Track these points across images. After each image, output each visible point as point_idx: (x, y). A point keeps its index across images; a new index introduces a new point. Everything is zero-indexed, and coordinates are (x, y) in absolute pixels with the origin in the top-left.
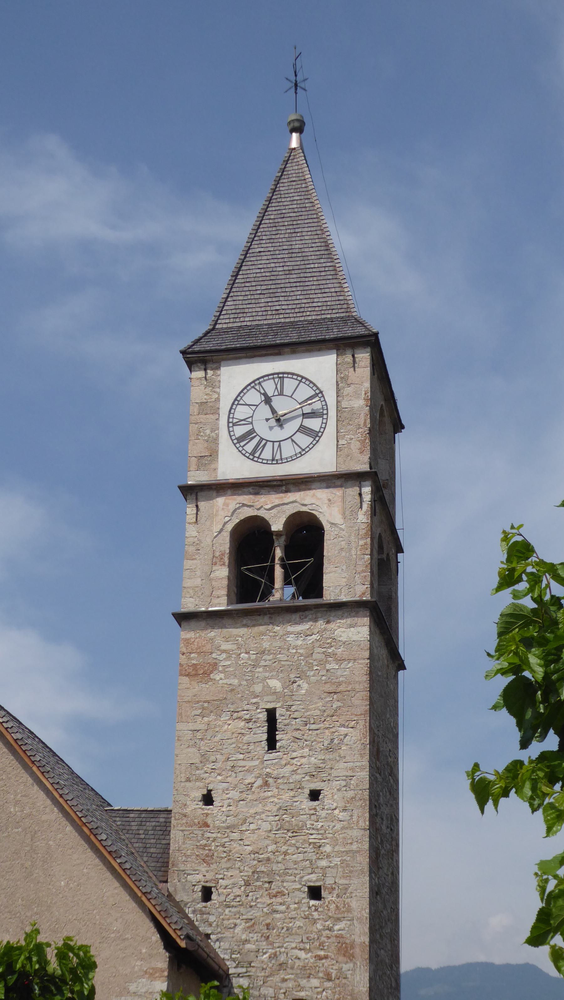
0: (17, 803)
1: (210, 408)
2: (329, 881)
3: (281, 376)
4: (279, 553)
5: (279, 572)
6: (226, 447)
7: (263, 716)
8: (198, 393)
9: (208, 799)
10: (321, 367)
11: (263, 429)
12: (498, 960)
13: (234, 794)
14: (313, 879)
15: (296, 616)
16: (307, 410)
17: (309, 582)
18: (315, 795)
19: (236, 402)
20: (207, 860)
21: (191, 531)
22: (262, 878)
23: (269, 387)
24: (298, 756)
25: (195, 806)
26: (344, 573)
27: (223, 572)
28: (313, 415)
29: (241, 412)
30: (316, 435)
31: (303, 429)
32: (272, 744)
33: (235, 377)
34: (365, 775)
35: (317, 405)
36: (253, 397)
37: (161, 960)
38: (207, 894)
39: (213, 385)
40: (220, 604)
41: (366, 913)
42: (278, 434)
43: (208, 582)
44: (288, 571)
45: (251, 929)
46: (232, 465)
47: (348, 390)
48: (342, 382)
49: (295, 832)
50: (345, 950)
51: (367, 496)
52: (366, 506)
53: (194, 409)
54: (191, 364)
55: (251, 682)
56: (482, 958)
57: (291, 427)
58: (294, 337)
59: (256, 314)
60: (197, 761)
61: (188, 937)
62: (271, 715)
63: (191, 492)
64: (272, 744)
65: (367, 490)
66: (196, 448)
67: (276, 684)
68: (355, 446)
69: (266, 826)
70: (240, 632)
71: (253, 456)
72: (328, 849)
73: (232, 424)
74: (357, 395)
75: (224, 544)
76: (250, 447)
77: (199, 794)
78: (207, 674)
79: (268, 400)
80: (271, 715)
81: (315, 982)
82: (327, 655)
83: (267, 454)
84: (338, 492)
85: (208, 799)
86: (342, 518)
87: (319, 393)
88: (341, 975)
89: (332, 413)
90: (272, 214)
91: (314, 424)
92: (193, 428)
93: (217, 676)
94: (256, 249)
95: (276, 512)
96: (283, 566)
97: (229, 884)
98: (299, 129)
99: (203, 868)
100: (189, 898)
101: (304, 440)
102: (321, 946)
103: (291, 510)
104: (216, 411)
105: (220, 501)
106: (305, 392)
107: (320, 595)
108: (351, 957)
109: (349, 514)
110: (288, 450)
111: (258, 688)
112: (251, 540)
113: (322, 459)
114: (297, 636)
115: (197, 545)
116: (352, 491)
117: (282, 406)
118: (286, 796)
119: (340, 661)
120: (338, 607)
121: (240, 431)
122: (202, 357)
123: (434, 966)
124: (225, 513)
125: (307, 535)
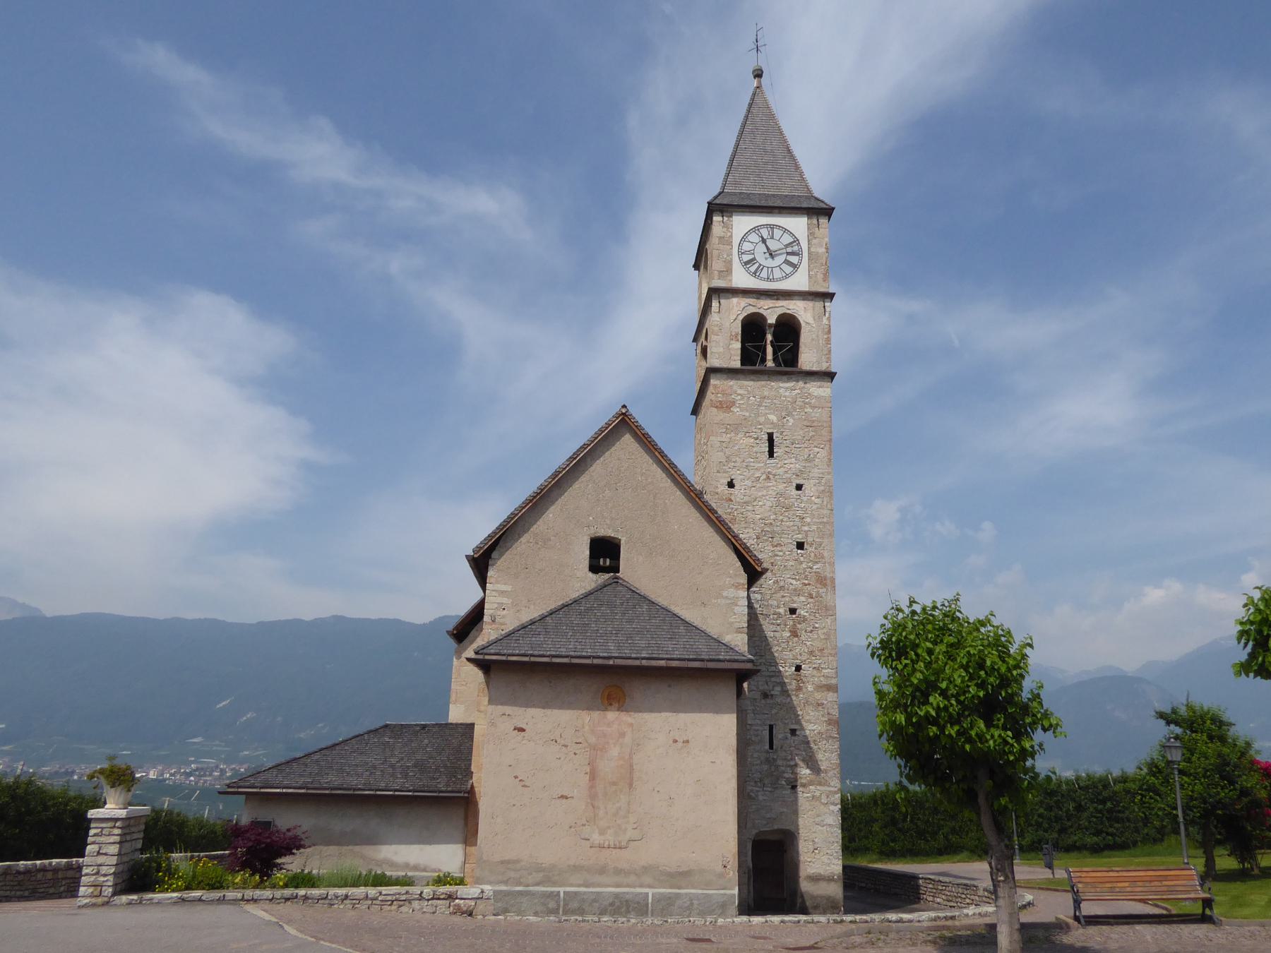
3: (772, 227)
5: (769, 350)
7: (766, 437)
9: (731, 485)
11: (761, 258)
13: (748, 483)
14: (800, 538)
15: (785, 378)
16: (789, 250)
19: (743, 239)
23: (765, 233)
27: (737, 345)
28: (793, 254)
31: (787, 262)
32: (771, 454)
36: (754, 238)
42: (770, 263)
46: (741, 279)
47: (814, 241)
49: (788, 508)
55: (758, 415)
57: (779, 260)
62: (770, 437)
64: (771, 454)
67: (773, 418)
69: (769, 504)
73: (741, 253)
76: (753, 269)
77: (726, 481)
78: (729, 408)
80: (770, 437)
81: (802, 599)
83: (764, 274)
87: (796, 241)
88: (818, 595)
89: (805, 254)
90: (749, 127)
91: (794, 259)
95: (771, 312)
101: (788, 269)
102: (806, 578)
103: (780, 311)
104: (730, 244)
105: (735, 300)
106: (787, 239)
111: (762, 419)
117: (773, 245)
118: (781, 487)
119: (814, 407)
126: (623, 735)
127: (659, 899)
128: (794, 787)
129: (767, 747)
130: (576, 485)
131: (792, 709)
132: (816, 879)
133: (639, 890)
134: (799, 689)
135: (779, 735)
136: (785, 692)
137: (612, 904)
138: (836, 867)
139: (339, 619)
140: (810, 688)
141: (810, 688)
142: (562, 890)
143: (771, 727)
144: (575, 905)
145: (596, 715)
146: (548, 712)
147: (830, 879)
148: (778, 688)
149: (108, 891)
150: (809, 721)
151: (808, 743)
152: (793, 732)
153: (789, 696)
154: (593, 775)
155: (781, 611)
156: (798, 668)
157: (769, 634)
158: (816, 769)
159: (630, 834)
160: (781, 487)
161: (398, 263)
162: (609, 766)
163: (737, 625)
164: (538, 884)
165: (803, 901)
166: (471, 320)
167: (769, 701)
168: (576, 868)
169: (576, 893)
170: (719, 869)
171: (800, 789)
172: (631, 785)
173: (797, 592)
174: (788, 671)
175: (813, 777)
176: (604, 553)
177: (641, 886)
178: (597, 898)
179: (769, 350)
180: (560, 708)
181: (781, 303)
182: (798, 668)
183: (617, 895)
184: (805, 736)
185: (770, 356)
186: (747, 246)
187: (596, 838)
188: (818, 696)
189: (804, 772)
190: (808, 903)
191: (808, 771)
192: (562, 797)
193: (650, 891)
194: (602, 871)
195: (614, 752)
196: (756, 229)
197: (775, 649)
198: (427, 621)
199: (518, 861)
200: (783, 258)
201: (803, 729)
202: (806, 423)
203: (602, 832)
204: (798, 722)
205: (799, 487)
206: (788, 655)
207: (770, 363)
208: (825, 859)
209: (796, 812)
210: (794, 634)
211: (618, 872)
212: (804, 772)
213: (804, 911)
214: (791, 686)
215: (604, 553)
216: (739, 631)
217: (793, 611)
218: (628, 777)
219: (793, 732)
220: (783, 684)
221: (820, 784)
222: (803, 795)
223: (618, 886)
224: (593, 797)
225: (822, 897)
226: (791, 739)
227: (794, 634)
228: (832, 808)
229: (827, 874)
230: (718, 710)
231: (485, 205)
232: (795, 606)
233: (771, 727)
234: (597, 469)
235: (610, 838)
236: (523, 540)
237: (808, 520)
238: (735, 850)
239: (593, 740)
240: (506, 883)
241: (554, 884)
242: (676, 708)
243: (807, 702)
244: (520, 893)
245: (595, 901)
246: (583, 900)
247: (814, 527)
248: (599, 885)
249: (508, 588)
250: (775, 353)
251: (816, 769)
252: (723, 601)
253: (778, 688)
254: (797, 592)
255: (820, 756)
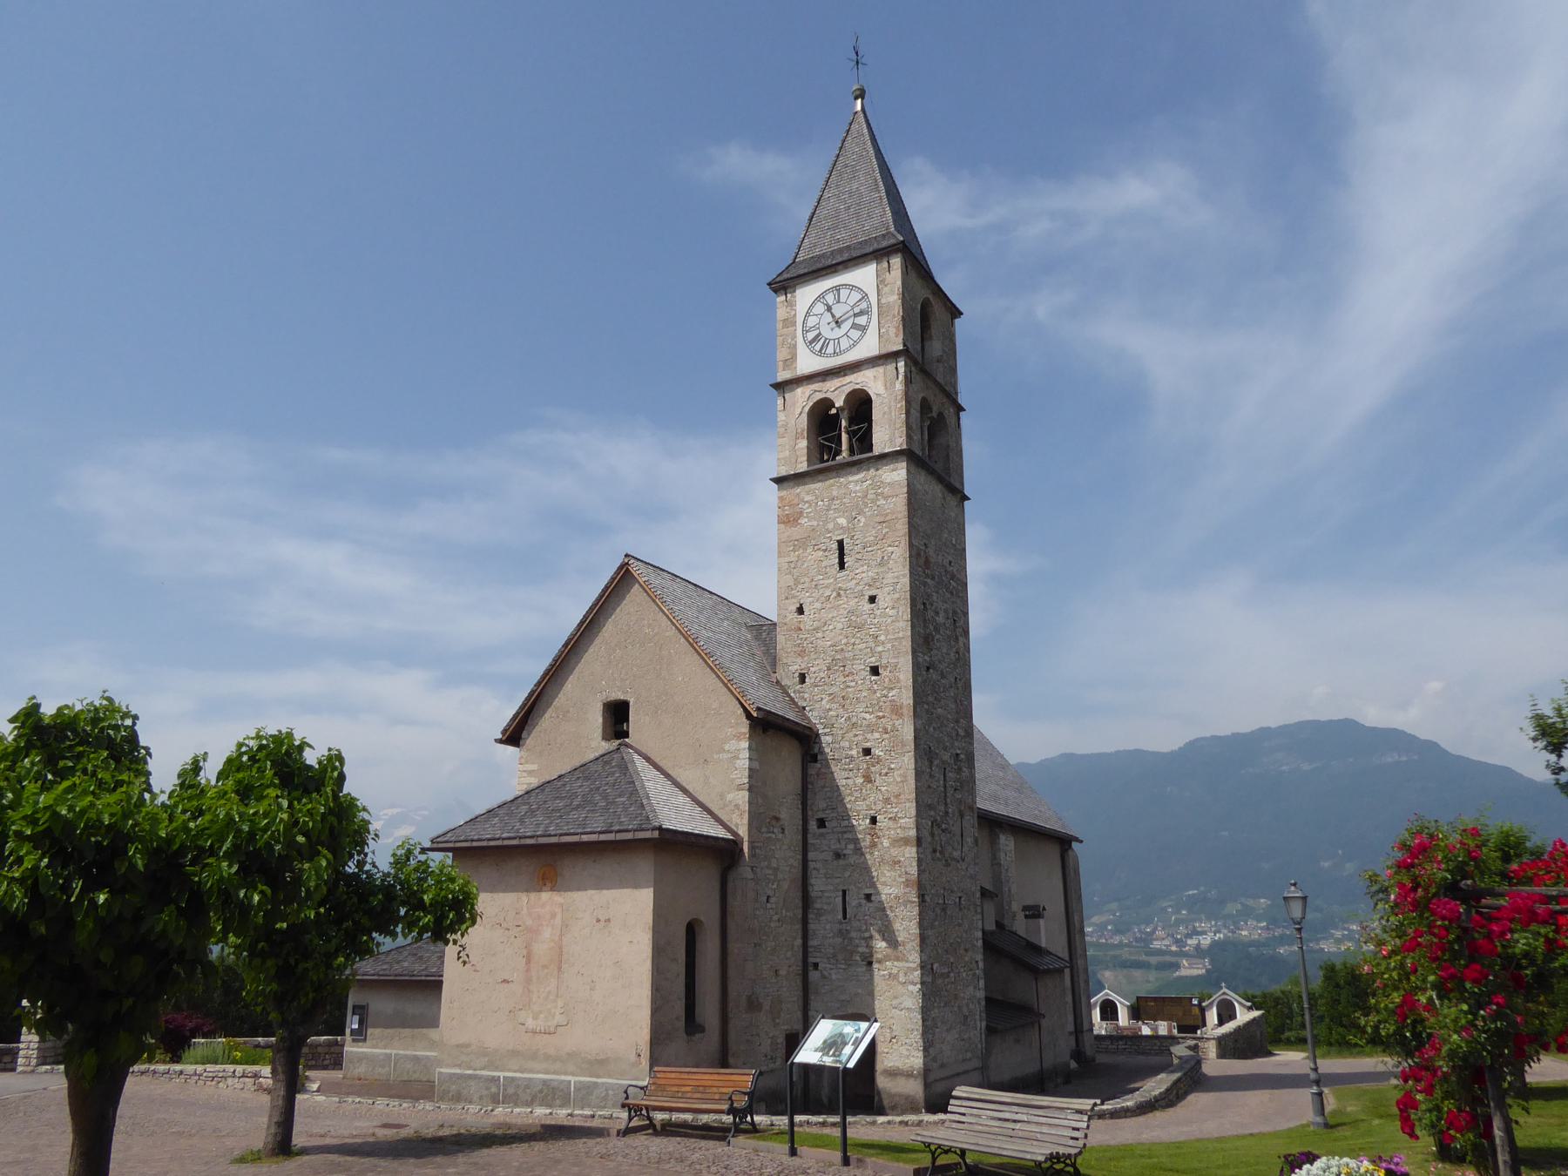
0: (649, 626)
1: (790, 322)
2: (884, 661)
3: (837, 289)
4: (844, 423)
5: (844, 437)
6: (802, 350)
7: (835, 546)
8: (782, 313)
9: (800, 611)
10: (865, 276)
11: (827, 332)
12: (1323, 718)
13: (818, 605)
14: (873, 661)
15: (854, 469)
16: (857, 310)
17: (863, 440)
18: (872, 599)
19: (808, 314)
20: (802, 654)
21: (781, 417)
22: (838, 664)
23: (830, 299)
24: (860, 572)
25: (792, 616)
26: (888, 432)
27: (803, 443)
28: (861, 313)
29: (812, 321)
30: (863, 329)
31: (855, 326)
32: (842, 565)
33: (806, 294)
34: (906, 580)
35: (864, 305)
36: (820, 308)
37: (744, 726)
38: (802, 678)
39: (791, 304)
40: (803, 467)
41: (910, 682)
42: (838, 333)
43: (795, 452)
44: (851, 434)
45: (832, 701)
46: (807, 362)
47: (886, 290)
48: (881, 283)
49: (860, 627)
50: (896, 710)
51: (902, 370)
52: (901, 377)
53: (779, 325)
54: (776, 291)
55: (826, 522)
56: (1310, 717)
57: (846, 326)
58: (846, 256)
59: (822, 245)
60: (791, 583)
61: (759, 709)
62: (841, 544)
63: (781, 387)
64: (842, 565)
65: (901, 364)
66: (782, 354)
67: (842, 521)
68: (892, 331)
69: (840, 626)
70: (816, 486)
71: (821, 353)
72: (882, 638)
73: (805, 331)
74: (892, 292)
75: (804, 422)
76: (818, 347)
77: (794, 608)
78: (796, 520)
79: (829, 309)
80: (841, 544)
81: (877, 735)
82: (877, 495)
83: (830, 350)
84: (881, 370)
85: (800, 611)
86: (886, 391)
87: (865, 296)
88: (894, 729)
89: (875, 310)
90: (839, 166)
91: (862, 320)
92: (780, 339)
93: (803, 521)
94: (826, 195)
95: (837, 392)
96: (848, 433)
97: (817, 670)
98: (861, 94)
99: (799, 660)
100: (791, 682)
101: (855, 334)
102: (880, 709)
103: (848, 389)
104: (794, 324)
105: (799, 391)
106: (856, 296)
107: (870, 449)
108: (901, 716)
109: (888, 386)
110: (845, 343)
111: (831, 526)
112: (823, 421)
113: (870, 346)
114: (856, 483)
115: (785, 426)
116: (891, 367)
117: (839, 311)
118: (853, 603)
119: (886, 498)
120: (883, 457)
121: (811, 336)
122: (783, 285)
123: (1273, 725)
124: (803, 399)
125: (861, 405)
126: (553, 916)
127: (581, 1087)
128: (870, 963)
129: (840, 916)
130: (591, 650)
131: (866, 869)
132: (893, 1073)
133: (563, 1077)
134: (873, 845)
135: (852, 902)
136: (859, 851)
137: (541, 1091)
138: (916, 1061)
139: (1069, 758)
140: (886, 843)
141: (886, 843)
142: (501, 1074)
143: (844, 892)
144: (511, 1091)
145: (533, 895)
146: (495, 895)
147: (909, 1075)
148: (851, 846)
149: (34, 1062)
150: (885, 884)
151: (884, 909)
152: (868, 897)
153: (863, 854)
154: (529, 958)
155: (854, 752)
156: (874, 820)
157: (841, 782)
158: (893, 942)
159: (559, 1019)
160: (853, 603)
161: (1043, 305)
162: (542, 949)
163: (739, 782)
164: (483, 1069)
165: (881, 1100)
166: (1155, 349)
167: (841, 862)
168: (514, 1053)
169: (513, 1079)
170: (633, 1057)
171: (875, 966)
172: (560, 968)
173: (871, 728)
174: (862, 824)
175: (889, 951)
176: (617, 716)
177: (566, 1073)
178: (529, 1083)
179: (844, 437)
180: (504, 891)
181: (848, 379)
182: (874, 820)
183: (545, 1082)
184: (881, 902)
185: (845, 446)
186: (812, 321)
187: (530, 1023)
188: (894, 852)
189: (880, 945)
190: (886, 1102)
191: (884, 944)
192: (504, 981)
193: (572, 1079)
194: (534, 1056)
195: (547, 933)
196: (821, 297)
197: (847, 799)
198: (1175, 748)
199: (468, 1046)
200: (848, 324)
201: (878, 893)
202: (878, 519)
203: (535, 1018)
204: (874, 885)
205: (872, 599)
206: (861, 805)
207: (845, 454)
208: (903, 1050)
209: (871, 994)
210: (868, 779)
211: (547, 1057)
212: (880, 945)
213: (882, 1112)
214: (866, 842)
215: (617, 716)
216: (740, 787)
217: (867, 752)
218: (559, 959)
219: (868, 897)
220: (856, 841)
221: (897, 959)
222: (879, 973)
223: (547, 1073)
224: (528, 981)
225: (900, 1095)
226: (868, 907)
227: (868, 779)
228: (911, 987)
229: (905, 1068)
230: (636, 886)
231: (1141, 193)
232: (868, 745)
233: (844, 892)
234: (610, 629)
235: (540, 1024)
236: (547, 715)
237: (882, 638)
238: (648, 1038)
239: (529, 922)
240: (459, 1066)
241: (497, 1069)
242: (600, 885)
243: (882, 861)
244: (470, 1077)
245: (527, 1087)
246: (518, 1086)
247: (889, 646)
248: (531, 1071)
249: (534, 767)
250: (850, 440)
251: (893, 942)
252: (725, 756)
253: (851, 846)
254: (871, 728)
255: (897, 926)
